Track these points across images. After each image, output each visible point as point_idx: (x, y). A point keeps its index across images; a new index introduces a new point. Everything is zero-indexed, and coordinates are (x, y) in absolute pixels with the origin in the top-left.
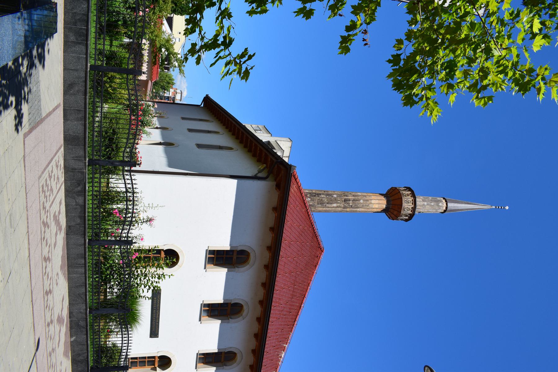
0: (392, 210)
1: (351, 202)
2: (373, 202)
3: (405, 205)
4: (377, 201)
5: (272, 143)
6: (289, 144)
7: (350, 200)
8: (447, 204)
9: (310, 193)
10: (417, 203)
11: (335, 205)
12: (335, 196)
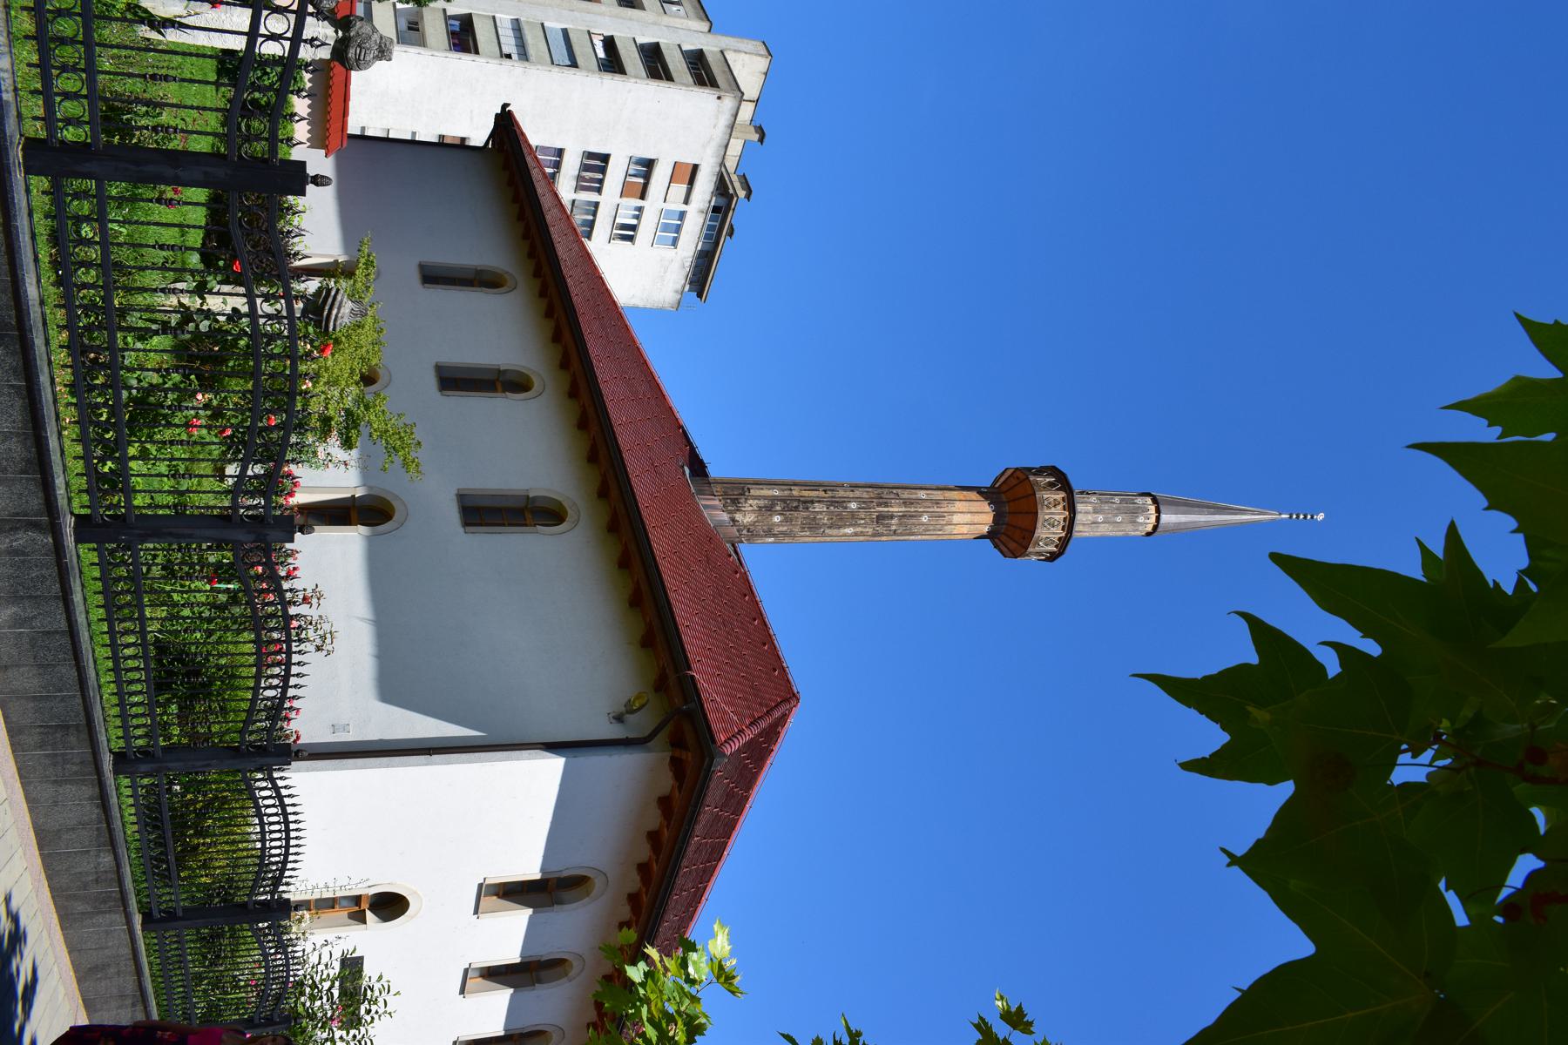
0: (1004, 538)
1: (895, 521)
2: (956, 518)
3: (1044, 515)
4: (968, 518)
5: (710, 59)
6: (762, 64)
7: (892, 517)
8: (1158, 511)
9: (783, 500)
11: (849, 531)
12: (853, 506)
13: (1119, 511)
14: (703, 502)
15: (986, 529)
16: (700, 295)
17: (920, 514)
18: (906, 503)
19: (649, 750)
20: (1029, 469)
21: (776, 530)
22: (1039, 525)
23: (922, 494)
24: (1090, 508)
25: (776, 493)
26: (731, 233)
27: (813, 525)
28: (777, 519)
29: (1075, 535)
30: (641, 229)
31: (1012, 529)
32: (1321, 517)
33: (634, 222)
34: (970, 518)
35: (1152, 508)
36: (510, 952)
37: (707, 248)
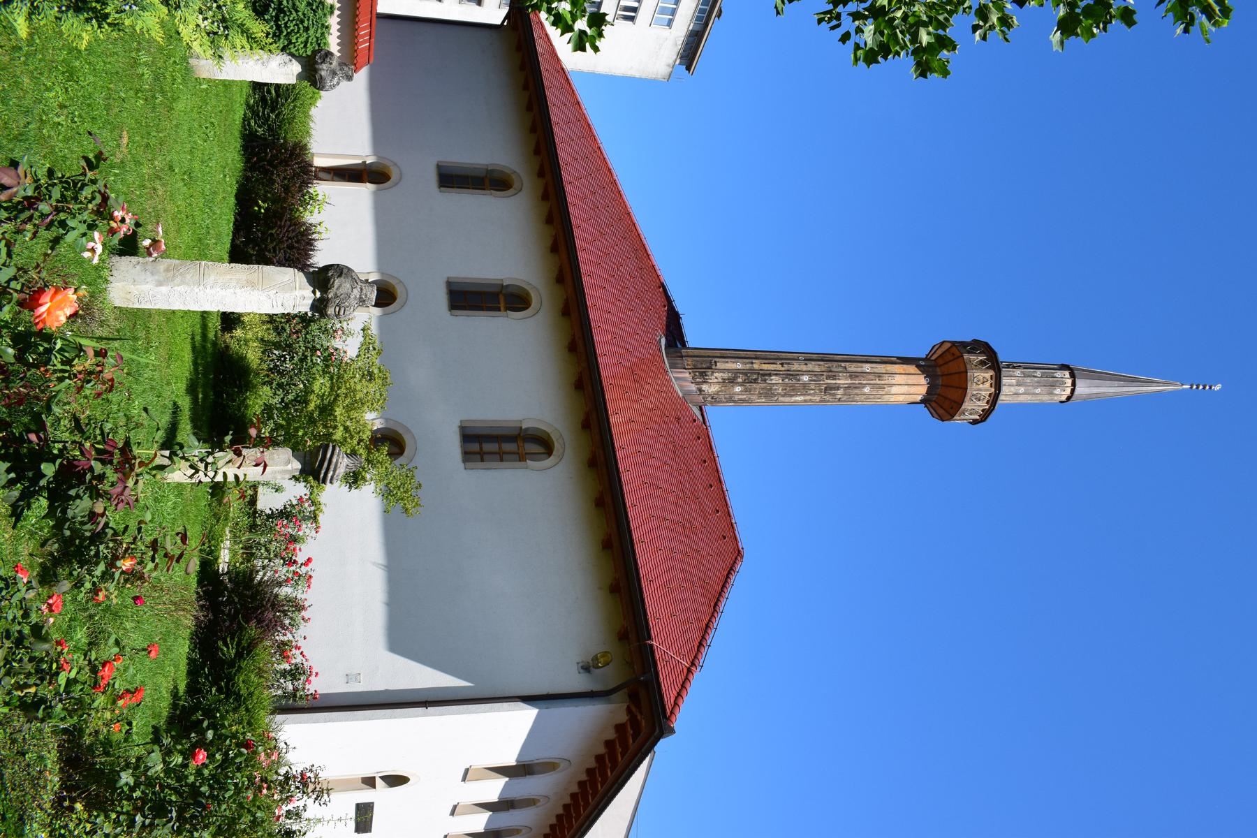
0: (934, 405)
2: (894, 390)
3: (972, 389)
4: (905, 389)
7: (838, 388)
8: (1074, 384)
10: (1004, 389)
11: (800, 398)
12: (805, 378)
13: (1039, 384)
14: (674, 375)
15: (919, 398)
16: (688, 69)
17: (864, 386)
18: (853, 376)
19: (610, 702)
20: (963, 344)
21: (736, 397)
22: (967, 398)
23: (867, 368)
24: (1014, 381)
25: (739, 366)
26: (719, 15)
27: (769, 394)
28: (738, 389)
29: (999, 402)
30: (641, 11)
31: (944, 397)
32: (1218, 387)
33: (636, 5)
34: (908, 387)
35: (1069, 382)
36: (494, 797)
37: (698, 28)
